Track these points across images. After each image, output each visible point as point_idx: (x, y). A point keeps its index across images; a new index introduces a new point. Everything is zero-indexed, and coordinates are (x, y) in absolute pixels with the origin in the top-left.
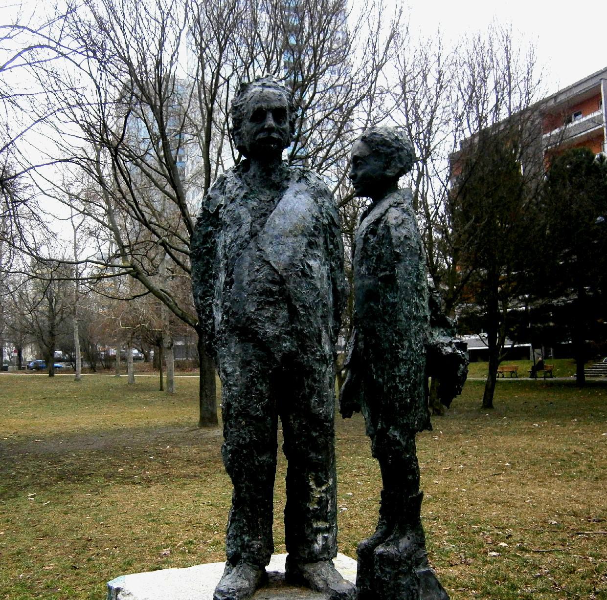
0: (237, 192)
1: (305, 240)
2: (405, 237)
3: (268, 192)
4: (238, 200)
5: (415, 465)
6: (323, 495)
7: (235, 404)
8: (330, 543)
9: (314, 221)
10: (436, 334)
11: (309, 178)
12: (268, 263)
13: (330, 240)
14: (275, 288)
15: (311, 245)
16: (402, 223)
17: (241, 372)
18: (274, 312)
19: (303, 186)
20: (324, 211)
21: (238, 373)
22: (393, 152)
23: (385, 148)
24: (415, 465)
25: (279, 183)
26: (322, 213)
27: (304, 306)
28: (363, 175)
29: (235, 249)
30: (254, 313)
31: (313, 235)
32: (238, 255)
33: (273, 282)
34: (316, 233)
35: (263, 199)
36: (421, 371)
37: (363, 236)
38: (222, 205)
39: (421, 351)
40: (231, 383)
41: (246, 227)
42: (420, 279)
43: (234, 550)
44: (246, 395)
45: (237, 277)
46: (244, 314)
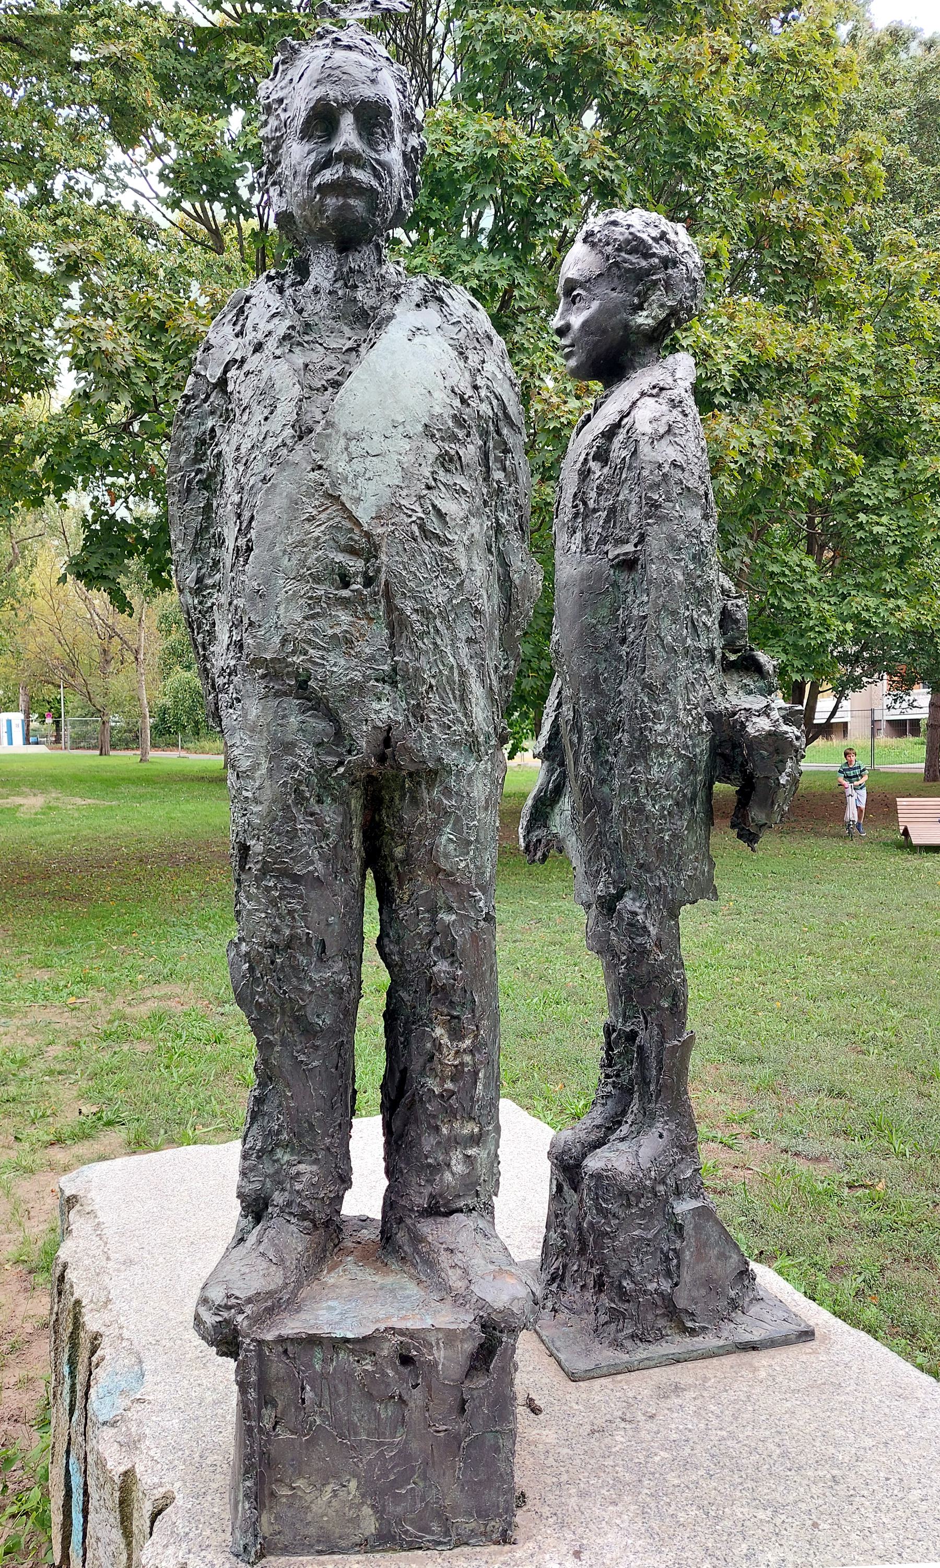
0: (270, 327)
1: (432, 450)
2: (674, 464)
3: (346, 329)
4: (271, 345)
5: (678, 976)
6: (467, 1058)
7: (256, 846)
8: (482, 1171)
9: (457, 403)
10: (732, 689)
11: (447, 300)
13: (497, 459)
14: (355, 565)
15: (446, 461)
16: (669, 431)
17: (270, 770)
19: (431, 316)
22: (652, 270)
23: (633, 258)
24: (678, 976)
27: (424, 612)
28: (585, 324)
30: (299, 624)
31: (454, 438)
33: (352, 551)
34: (461, 434)
36: (694, 772)
37: (579, 465)
38: (236, 361)
39: (698, 726)
40: (249, 794)
41: (286, 411)
42: (704, 564)
43: (258, 1186)
45: (259, 534)
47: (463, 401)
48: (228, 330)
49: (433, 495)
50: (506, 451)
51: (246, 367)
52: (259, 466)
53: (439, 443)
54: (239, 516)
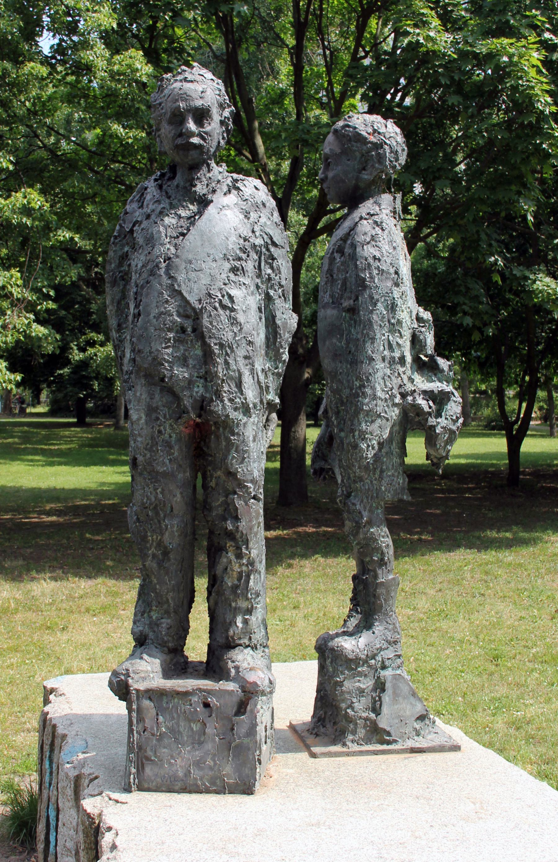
0: (154, 207)
1: (227, 266)
2: (375, 258)
9: (242, 241)
12: (180, 293)
17: (146, 421)
18: (185, 350)
20: (257, 228)
21: (143, 421)
22: (369, 151)
25: (204, 195)
26: (253, 232)
27: (221, 346)
28: (333, 178)
29: (145, 275)
31: (240, 259)
32: (148, 282)
34: (244, 256)
35: (183, 215)
43: (141, 628)
44: (152, 447)
45: (144, 308)
46: (151, 352)
47: (245, 240)
48: (135, 205)
49: (227, 288)
50: (273, 259)
51: (142, 226)
52: (145, 275)
53: (232, 262)
54: (136, 299)
